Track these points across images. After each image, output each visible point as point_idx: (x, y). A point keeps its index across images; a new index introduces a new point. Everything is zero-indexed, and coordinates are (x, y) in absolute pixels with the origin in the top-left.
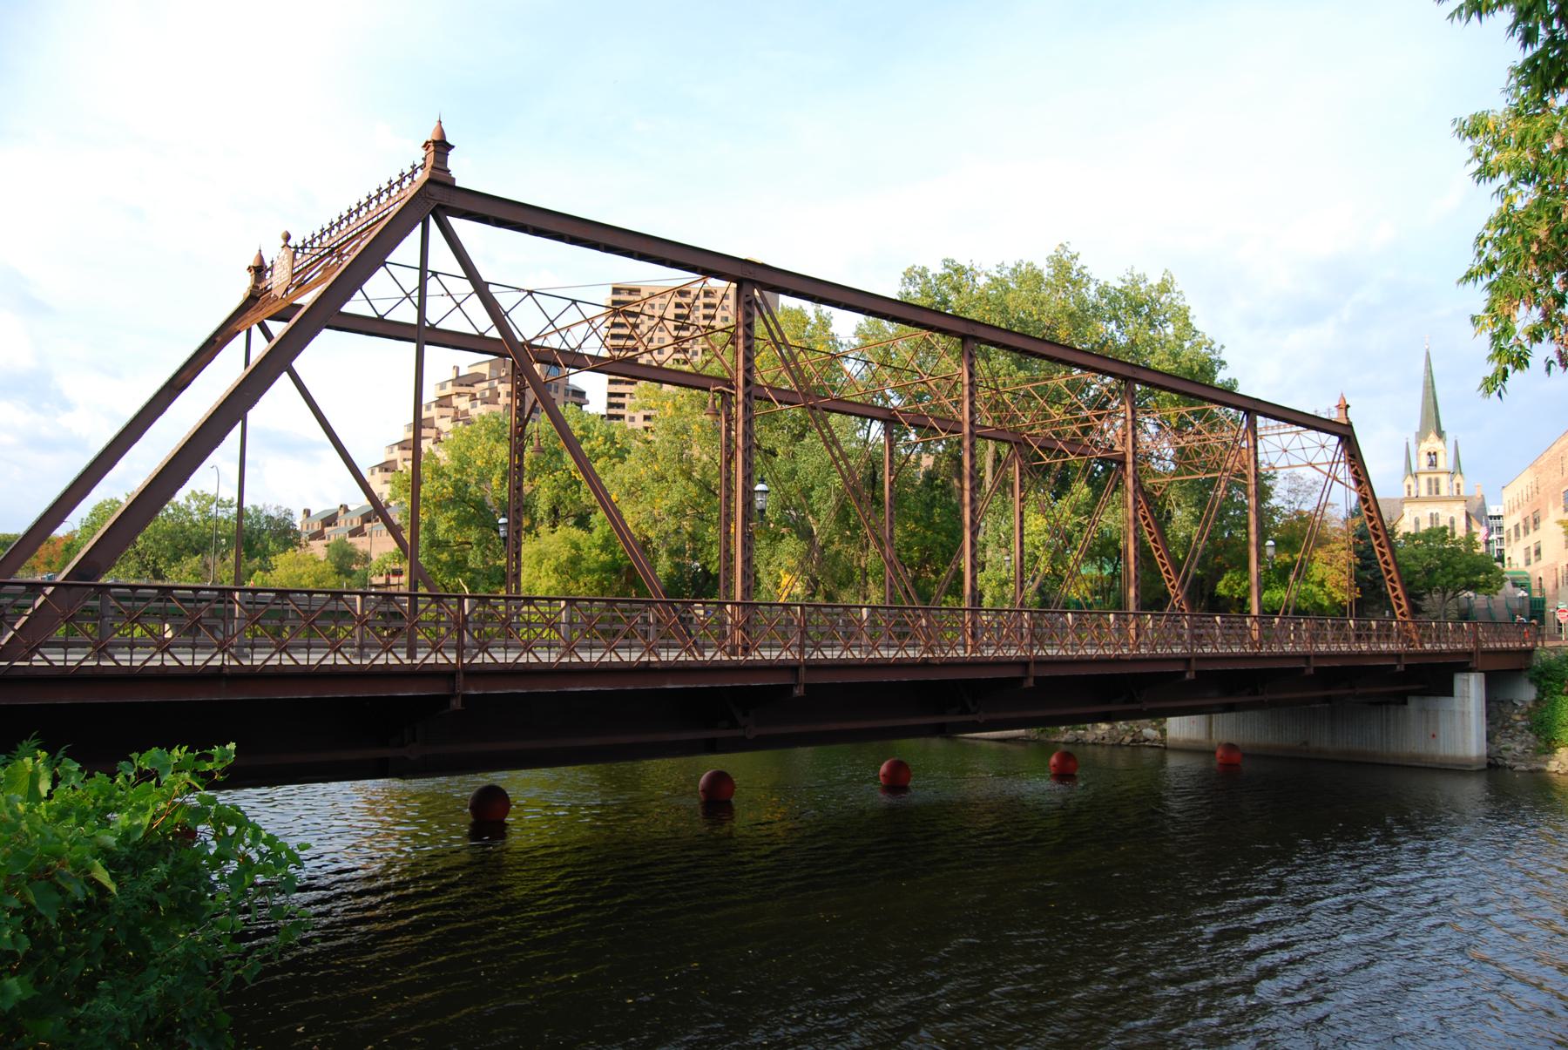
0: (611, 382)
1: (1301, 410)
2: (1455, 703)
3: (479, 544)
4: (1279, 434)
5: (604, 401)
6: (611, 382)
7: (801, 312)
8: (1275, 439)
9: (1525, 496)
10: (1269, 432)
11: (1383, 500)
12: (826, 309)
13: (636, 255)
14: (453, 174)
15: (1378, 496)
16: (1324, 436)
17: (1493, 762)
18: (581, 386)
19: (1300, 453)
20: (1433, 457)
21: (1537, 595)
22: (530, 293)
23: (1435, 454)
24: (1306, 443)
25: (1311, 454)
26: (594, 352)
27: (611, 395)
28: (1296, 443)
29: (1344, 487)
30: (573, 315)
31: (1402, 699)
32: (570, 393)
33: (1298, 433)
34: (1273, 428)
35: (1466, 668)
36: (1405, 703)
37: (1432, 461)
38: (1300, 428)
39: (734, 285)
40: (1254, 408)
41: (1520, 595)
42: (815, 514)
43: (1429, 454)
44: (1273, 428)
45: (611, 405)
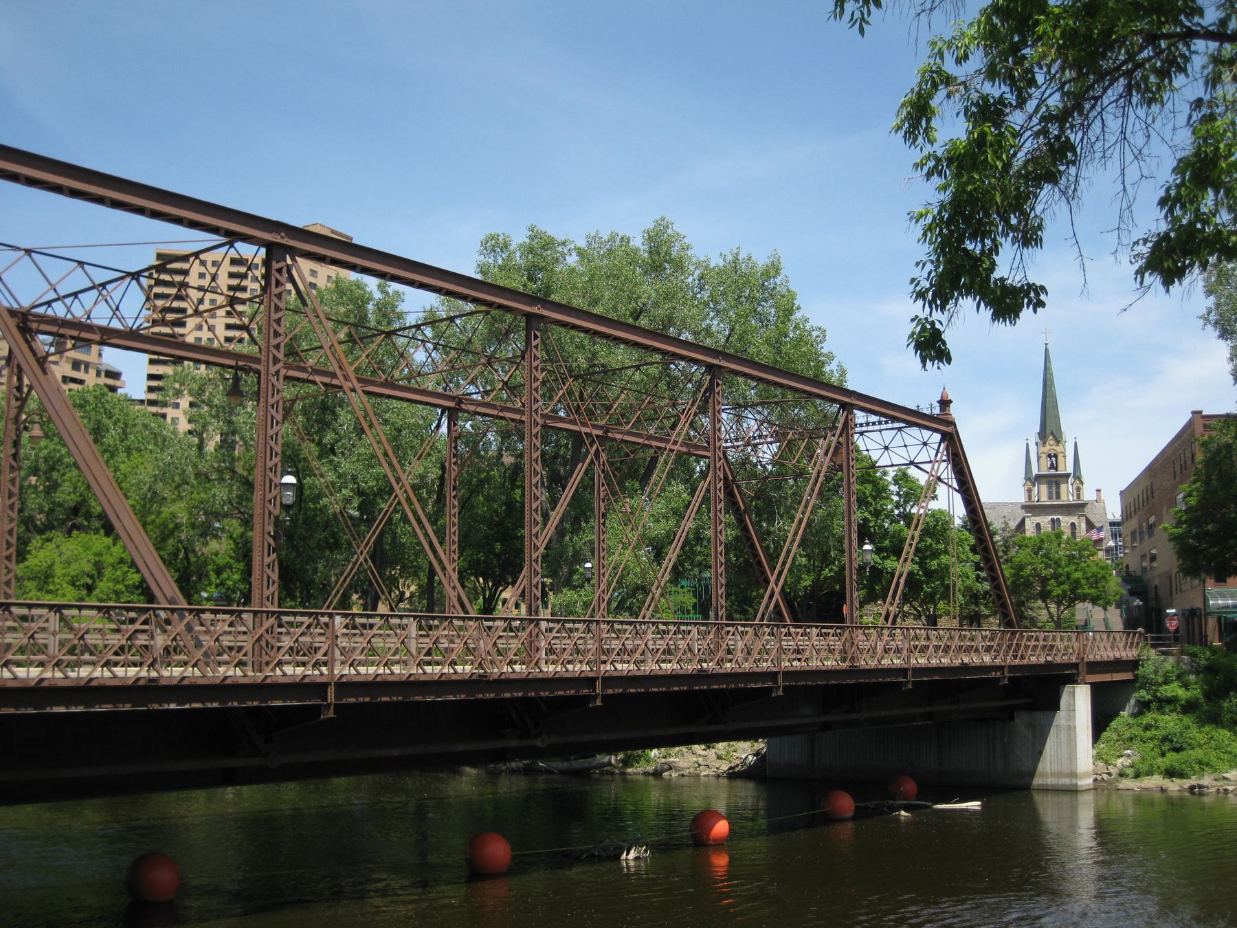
0: (152, 362)
1: (902, 405)
2: (1061, 717)
3: (337, 637)
4: (880, 431)
5: (145, 383)
6: (152, 362)
7: (358, 285)
8: (876, 436)
9: (1141, 501)
10: (870, 428)
11: (995, 506)
12: (394, 286)
13: (107, 201)
14: (954, 416)
15: (982, 501)
16: (926, 433)
17: (1099, 777)
18: (116, 366)
19: (902, 451)
20: (1053, 459)
21: (1153, 603)
22: (29, 252)
23: (1056, 456)
24: (909, 441)
25: (913, 452)
26: (104, 323)
27: (151, 377)
28: (898, 441)
29: (946, 487)
30: (79, 280)
31: (1008, 715)
32: (103, 374)
33: (899, 429)
34: (874, 424)
35: (1072, 680)
36: (1012, 719)
37: (1052, 464)
38: (902, 425)
39: (263, 251)
40: (851, 401)
41: (1135, 604)
42: (82, 417)
43: (1050, 456)
44: (874, 424)
45: (151, 389)
